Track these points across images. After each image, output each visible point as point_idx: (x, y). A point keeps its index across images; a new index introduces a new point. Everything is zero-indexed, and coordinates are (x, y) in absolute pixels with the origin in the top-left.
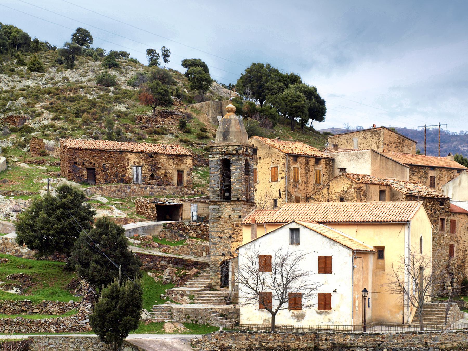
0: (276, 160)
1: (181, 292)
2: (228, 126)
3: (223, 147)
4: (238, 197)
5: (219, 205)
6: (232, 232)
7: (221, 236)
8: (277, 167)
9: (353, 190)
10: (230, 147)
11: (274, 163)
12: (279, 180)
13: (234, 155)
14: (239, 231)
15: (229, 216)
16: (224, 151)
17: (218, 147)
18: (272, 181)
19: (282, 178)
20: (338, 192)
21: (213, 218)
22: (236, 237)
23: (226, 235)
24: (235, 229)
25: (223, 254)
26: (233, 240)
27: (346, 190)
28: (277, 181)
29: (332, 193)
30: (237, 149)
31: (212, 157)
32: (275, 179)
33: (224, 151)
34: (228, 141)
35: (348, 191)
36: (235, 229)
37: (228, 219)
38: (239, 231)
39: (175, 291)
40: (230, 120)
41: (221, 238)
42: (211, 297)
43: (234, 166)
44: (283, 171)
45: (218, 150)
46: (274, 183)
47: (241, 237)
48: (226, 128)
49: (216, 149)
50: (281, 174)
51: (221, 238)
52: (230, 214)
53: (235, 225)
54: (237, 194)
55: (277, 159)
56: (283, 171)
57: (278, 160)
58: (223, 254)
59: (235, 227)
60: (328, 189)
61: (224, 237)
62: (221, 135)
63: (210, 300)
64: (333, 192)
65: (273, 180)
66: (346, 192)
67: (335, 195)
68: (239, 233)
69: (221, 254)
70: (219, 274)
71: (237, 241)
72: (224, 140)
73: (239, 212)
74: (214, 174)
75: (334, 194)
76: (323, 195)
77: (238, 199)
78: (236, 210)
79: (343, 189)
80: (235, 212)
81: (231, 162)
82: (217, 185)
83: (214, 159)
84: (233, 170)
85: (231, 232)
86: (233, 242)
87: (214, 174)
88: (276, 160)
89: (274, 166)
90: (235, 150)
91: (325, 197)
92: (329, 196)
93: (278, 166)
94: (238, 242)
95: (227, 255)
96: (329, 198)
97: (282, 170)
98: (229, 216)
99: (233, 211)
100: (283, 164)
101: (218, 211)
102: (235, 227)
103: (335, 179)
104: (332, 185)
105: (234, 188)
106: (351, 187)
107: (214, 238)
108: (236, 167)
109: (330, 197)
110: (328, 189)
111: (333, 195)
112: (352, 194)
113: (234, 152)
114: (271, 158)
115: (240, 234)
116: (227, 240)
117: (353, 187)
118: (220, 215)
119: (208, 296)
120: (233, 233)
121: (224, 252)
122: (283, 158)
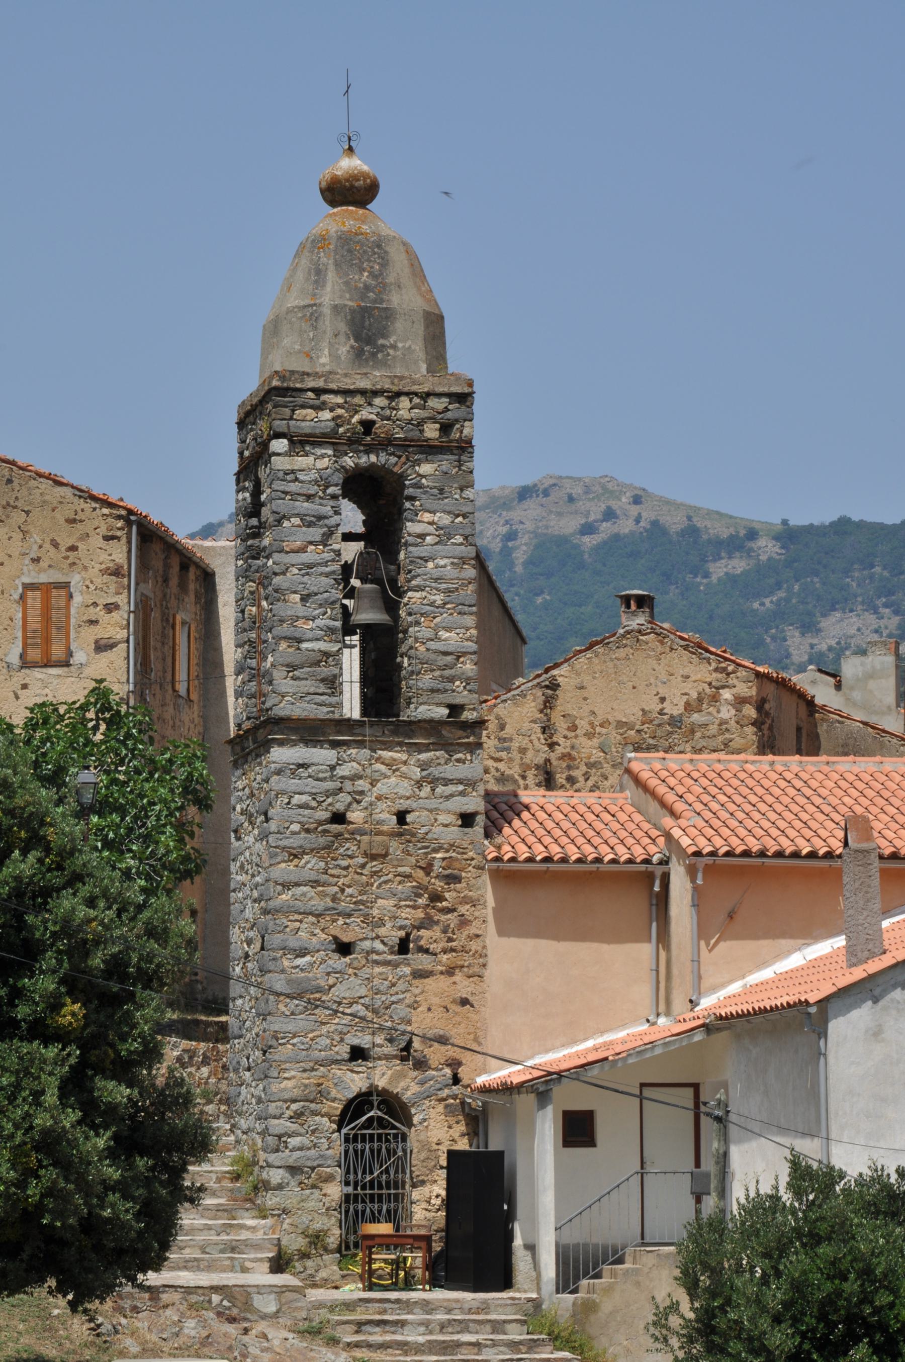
0: (55, 544)
1: (216, 1298)
2: (372, 275)
3: (358, 400)
4: (458, 701)
5: (335, 745)
6: (420, 914)
7: (345, 939)
8: (66, 585)
9: (727, 713)
10: (404, 402)
11: (44, 564)
12: (79, 657)
13: (430, 450)
14: (464, 909)
15: (401, 817)
16: (363, 423)
17: (325, 397)
18: (26, 664)
19: (102, 647)
20: (620, 724)
21: (295, 827)
22: (443, 944)
23: (382, 931)
24: (436, 897)
25: (358, 1054)
26: (423, 961)
27: (675, 708)
28: (67, 665)
29: (574, 728)
30: (449, 415)
31: (288, 454)
32: (47, 652)
33: (368, 425)
34: (384, 364)
35: (696, 717)
36: (436, 897)
37: (393, 835)
38: (464, 909)
39: (176, 1297)
40: (379, 246)
41: (344, 949)
42: (443, 1327)
43: (427, 517)
44: (110, 608)
45: (326, 415)
46: (38, 674)
47: (474, 946)
48: (367, 288)
49: (318, 408)
50: (93, 622)
51: (344, 949)
52: (403, 805)
53: (437, 868)
54: (451, 680)
55: (65, 542)
56: (110, 608)
57: (73, 548)
58: (358, 1054)
59: (439, 884)
60: (548, 704)
61: (367, 945)
62: (343, 327)
63: (458, 1345)
64: (583, 725)
65: (34, 654)
66: (675, 722)
67: (596, 742)
68: (464, 922)
69: (344, 1051)
70: (329, 1178)
71: (450, 972)
72: (358, 354)
73: (462, 794)
74: (304, 558)
75: (589, 735)
76: (502, 740)
77: (455, 709)
78: (447, 782)
79: (654, 706)
80: (440, 789)
81: (409, 492)
82: (319, 622)
83: (302, 462)
84: (422, 536)
85: (409, 916)
86: (420, 975)
87: (304, 558)
88: (55, 544)
89: (43, 578)
90: (433, 419)
91: (523, 751)
92: (552, 746)
93: (75, 580)
94: (458, 977)
95: (387, 1057)
96: (553, 756)
97: (102, 601)
98: (401, 817)
99: (427, 789)
100: (106, 572)
101: (330, 785)
102: (439, 884)
103: (598, 649)
104: (575, 681)
105: (432, 645)
106: (715, 698)
107: (302, 953)
108: (445, 520)
109: (559, 750)
110: (548, 704)
111: (583, 740)
112: (721, 732)
113: (431, 432)
114: (24, 533)
115: (473, 930)
116: (387, 963)
117: (726, 694)
118: (340, 807)
119: (426, 1324)
120: (427, 923)
121: (364, 1040)
122: (107, 538)
